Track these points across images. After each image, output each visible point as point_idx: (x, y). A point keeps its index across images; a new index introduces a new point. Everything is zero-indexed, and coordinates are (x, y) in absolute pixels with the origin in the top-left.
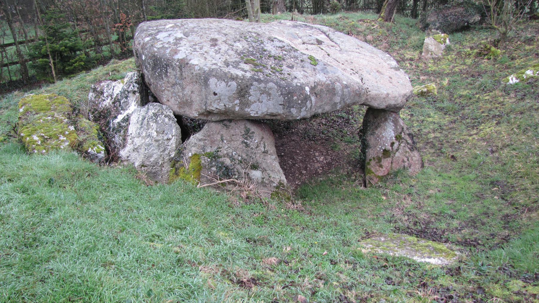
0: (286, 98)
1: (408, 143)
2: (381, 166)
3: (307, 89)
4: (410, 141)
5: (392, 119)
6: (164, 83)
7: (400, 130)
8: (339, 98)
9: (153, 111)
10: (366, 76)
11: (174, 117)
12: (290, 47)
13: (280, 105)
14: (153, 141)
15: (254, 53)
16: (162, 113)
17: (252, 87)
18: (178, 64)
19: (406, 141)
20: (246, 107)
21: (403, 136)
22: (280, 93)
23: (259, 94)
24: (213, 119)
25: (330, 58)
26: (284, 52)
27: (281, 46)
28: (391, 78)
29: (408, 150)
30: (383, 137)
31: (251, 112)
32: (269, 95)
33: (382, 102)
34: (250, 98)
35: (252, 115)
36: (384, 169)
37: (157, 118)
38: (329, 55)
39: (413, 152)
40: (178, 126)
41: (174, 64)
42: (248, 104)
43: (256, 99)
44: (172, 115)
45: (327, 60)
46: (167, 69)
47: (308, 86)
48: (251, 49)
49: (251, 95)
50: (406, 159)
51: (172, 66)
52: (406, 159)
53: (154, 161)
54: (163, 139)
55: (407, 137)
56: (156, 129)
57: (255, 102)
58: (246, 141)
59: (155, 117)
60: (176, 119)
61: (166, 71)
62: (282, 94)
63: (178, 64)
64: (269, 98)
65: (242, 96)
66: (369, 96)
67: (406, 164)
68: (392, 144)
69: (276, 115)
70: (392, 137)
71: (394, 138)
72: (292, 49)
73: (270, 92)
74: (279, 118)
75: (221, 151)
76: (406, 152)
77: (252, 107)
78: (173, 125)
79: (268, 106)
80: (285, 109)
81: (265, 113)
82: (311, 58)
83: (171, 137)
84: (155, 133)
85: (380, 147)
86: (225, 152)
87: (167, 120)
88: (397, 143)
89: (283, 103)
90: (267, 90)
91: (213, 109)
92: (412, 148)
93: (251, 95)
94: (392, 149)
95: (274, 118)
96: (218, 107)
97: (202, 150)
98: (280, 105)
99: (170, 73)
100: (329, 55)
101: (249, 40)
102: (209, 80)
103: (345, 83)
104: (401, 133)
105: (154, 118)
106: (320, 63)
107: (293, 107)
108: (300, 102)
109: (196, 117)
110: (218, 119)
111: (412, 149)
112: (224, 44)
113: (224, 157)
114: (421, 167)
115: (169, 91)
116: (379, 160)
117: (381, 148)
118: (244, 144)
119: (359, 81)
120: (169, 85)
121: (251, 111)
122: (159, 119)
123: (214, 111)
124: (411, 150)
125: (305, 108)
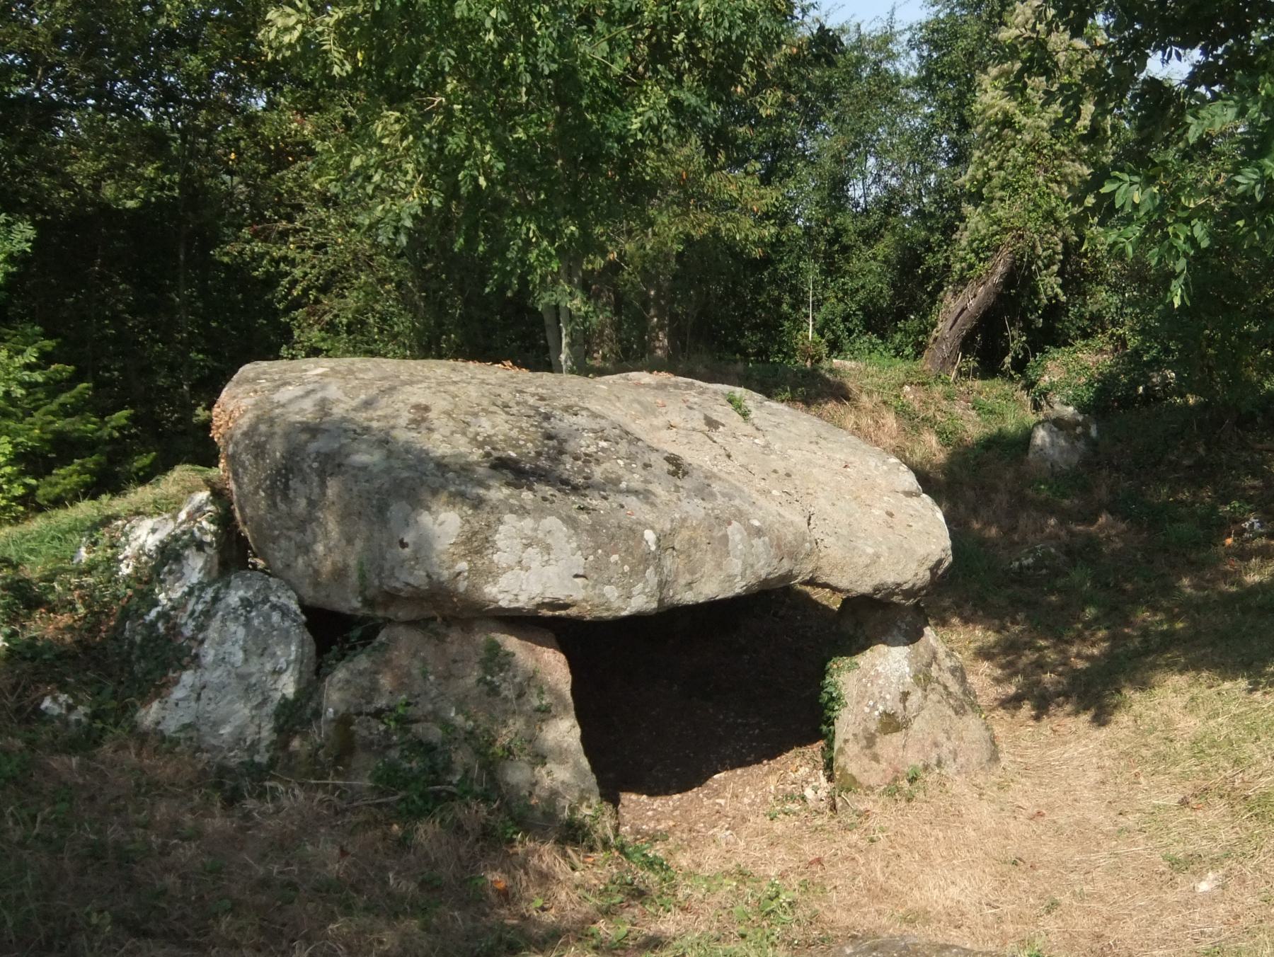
0: (591, 558)
1: (949, 694)
2: (876, 758)
3: (650, 536)
4: (955, 688)
5: (904, 626)
6: (278, 518)
7: (927, 658)
8: (740, 563)
9: (241, 593)
10: (821, 504)
11: (299, 611)
12: (617, 431)
13: (577, 576)
14: (233, 675)
15: (522, 443)
16: (266, 600)
17: (501, 528)
18: (315, 465)
19: (946, 688)
20: (487, 582)
21: (934, 674)
22: (574, 545)
23: (520, 547)
24: (402, 615)
25: (730, 463)
26: (603, 444)
27: (597, 427)
28: (891, 515)
29: (951, 712)
30: (878, 675)
31: (500, 596)
32: (548, 549)
33: (862, 576)
34: (495, 557)
35: (503, 604)
36: (884, 765)
37: (250, 612)
38: (729, 456)
39: (964, 718)
40: (307, 636)
41: (305, 466)
42: (492, 574)
43: (512, 560)
44: (294, 606)
45: (722, 467)
46: (288, 480)
47: (652, 528)
48: (514, 433)
49: (498, 550)
50: (941, 737)
51: (301, 470)
52: (941, 737)
53: (231, 734)
54: (260, 671)
55: (948, 675)
56: (245, 641)
57: (511, 568)
58: (489, 678)
59: (245, 608)
60: (304, 617)
61: (287, 486)
62: (579, 548)
63: (315, 465)
64: (546, 558)
65: (477, 552)
66: (825, 560)
67: (944, 751)
68: (905, 696)
69: (566, 606)
70: (902, 676)
71: (908, 679)
72: (624, 435)
73: (549, 541)
74: (573, 612)
75: (417, 703)
76: (943, 717)
77: (503, 581)
78: (295, 631)
79: (544, 579)
80: (589, 589)
81: (538, 600)
82: (673, 460)
83: (284, 666)
84: (241, 655)
85: (871, 703)
86: (430, 707)
87: (276, 617)
88: (919, 693)
89: (581, 572)
90: (541, 535)
91: (398, 585)
92: (963, 707)
93: (498, 550)
94: (905, 708)
95: (563, 613)
96: (411, 580)
97: (363, 701)
98: (577, 576)
99: (295, 490)
100: (729, 456)
101: (514, 410)
102: (388, 506)
103: (756, 523)
104: (929, 665)
105: (241, 611)
106: (695, 474)
107: (609, 583)
108: (626, 568)
109: (356, 609)
110: (414, 616)
111: (959, 711)
112: (444, 419)
113: (426, 721)
114: (990, 760)
115: (290, 539)
116: (870, 741)
117: (874, 708)
118: (486, 688)
119: (800, 521)
120: (291, 524)
121: (501, 592)
122: (253, 614)
123: (400, 590)
124: (957, 713)
125: (640, 586)
